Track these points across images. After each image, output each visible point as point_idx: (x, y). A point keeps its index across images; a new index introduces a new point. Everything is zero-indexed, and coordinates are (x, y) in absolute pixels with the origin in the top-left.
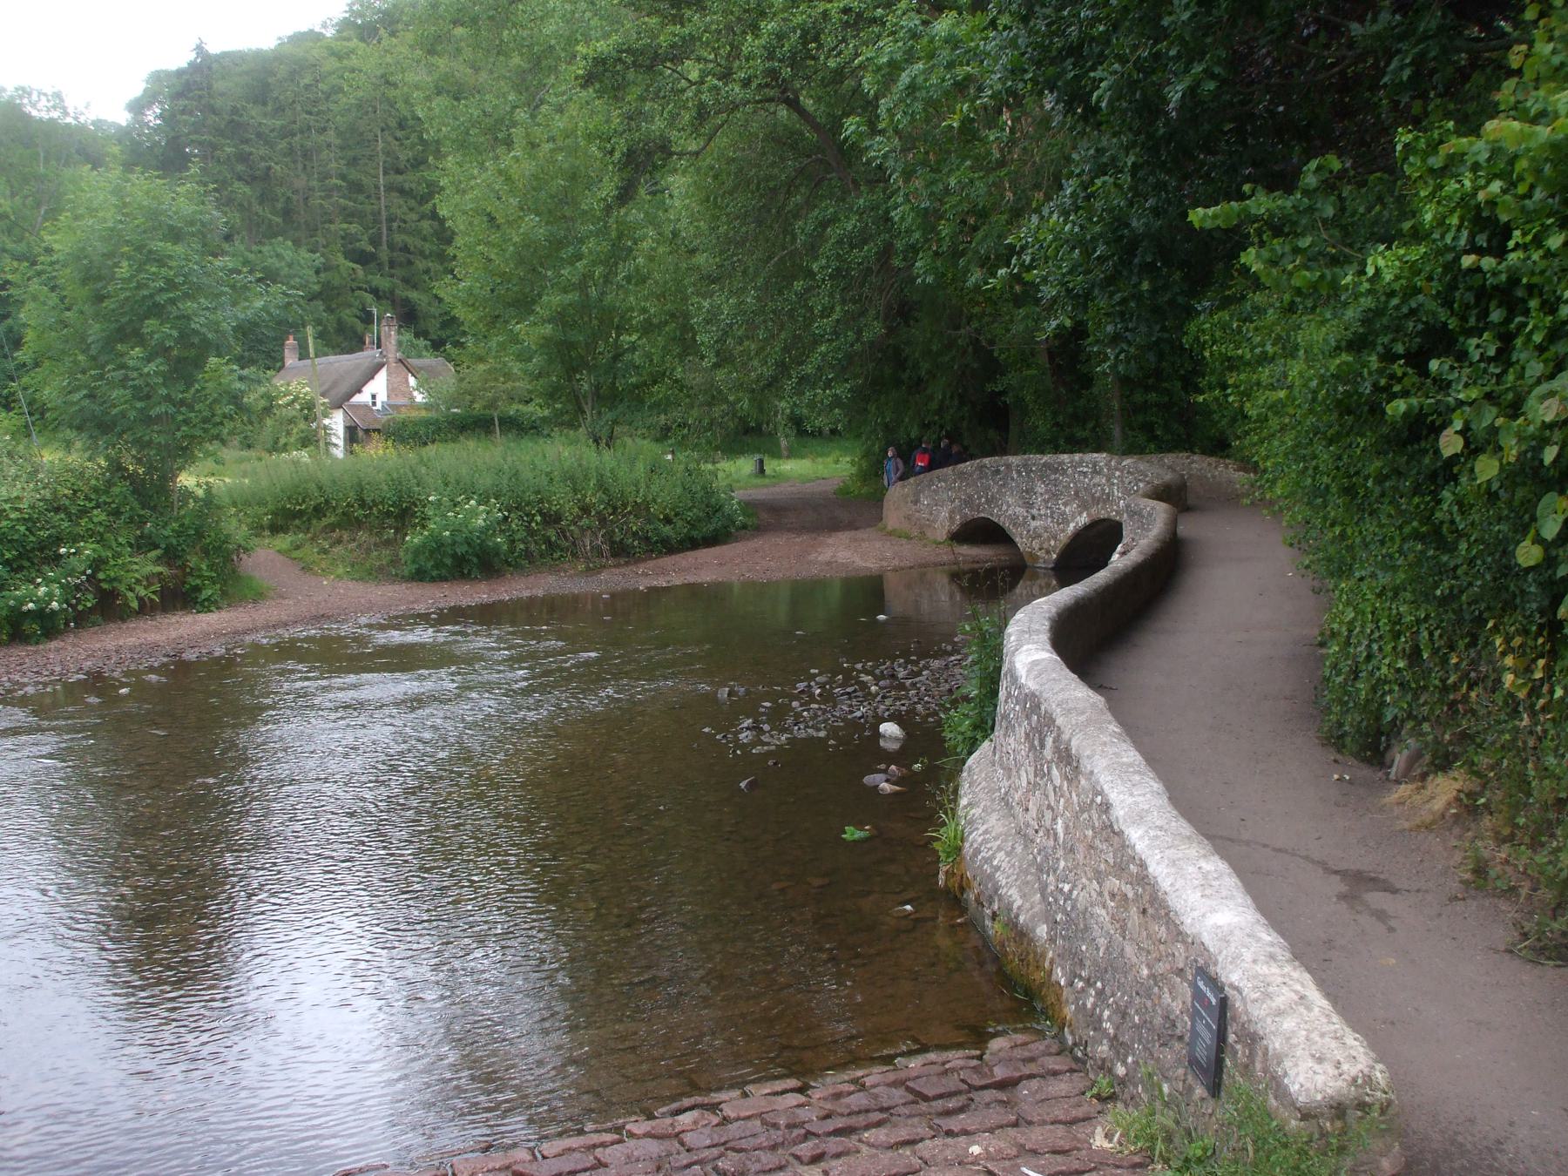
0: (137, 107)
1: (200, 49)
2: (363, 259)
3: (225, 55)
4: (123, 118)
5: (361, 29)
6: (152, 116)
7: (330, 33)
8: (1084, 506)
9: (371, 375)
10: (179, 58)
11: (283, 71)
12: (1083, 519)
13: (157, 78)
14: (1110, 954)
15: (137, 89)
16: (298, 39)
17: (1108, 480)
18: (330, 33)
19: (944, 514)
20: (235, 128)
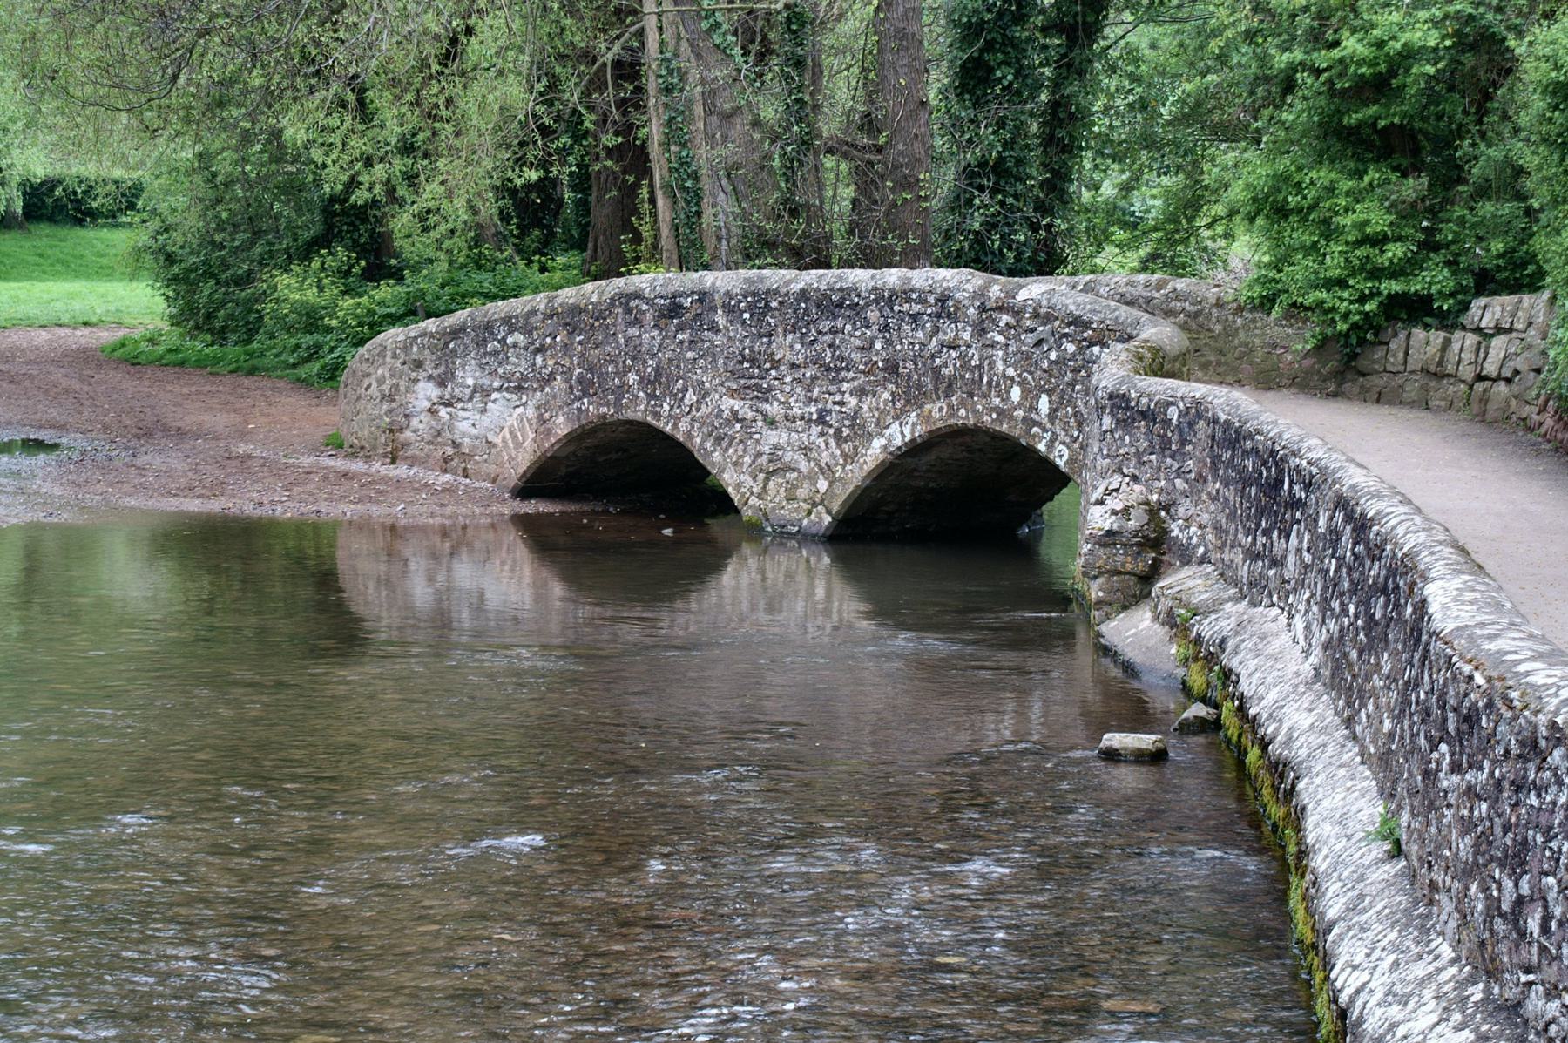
8: (912, 397)
12: (900, 433)
17: (980, 331)
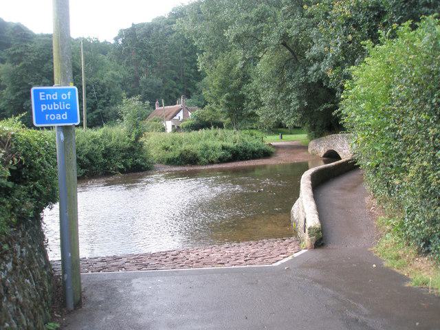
0: (116, 39)
1: (133, 24)
2: (175, 79)
3: (43, 36)
4: (113, 42)
5: (197, 13)
6: (120, 42)
7: (167, 17)
9: (178, 111)
10: (127, 25)
11: (141, 32)
13: (121, 31)
14: (429, 185)
15: (116, 34)
16: (158, 19)
18: (167, 17)
19: (323, 149)
20: (141, 45)
